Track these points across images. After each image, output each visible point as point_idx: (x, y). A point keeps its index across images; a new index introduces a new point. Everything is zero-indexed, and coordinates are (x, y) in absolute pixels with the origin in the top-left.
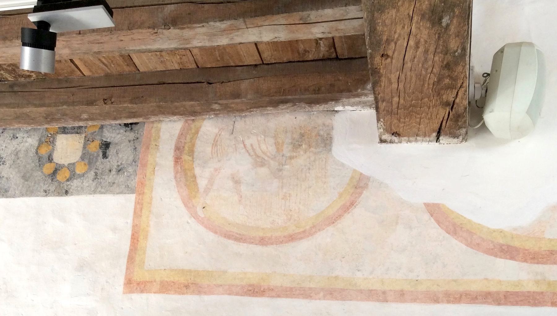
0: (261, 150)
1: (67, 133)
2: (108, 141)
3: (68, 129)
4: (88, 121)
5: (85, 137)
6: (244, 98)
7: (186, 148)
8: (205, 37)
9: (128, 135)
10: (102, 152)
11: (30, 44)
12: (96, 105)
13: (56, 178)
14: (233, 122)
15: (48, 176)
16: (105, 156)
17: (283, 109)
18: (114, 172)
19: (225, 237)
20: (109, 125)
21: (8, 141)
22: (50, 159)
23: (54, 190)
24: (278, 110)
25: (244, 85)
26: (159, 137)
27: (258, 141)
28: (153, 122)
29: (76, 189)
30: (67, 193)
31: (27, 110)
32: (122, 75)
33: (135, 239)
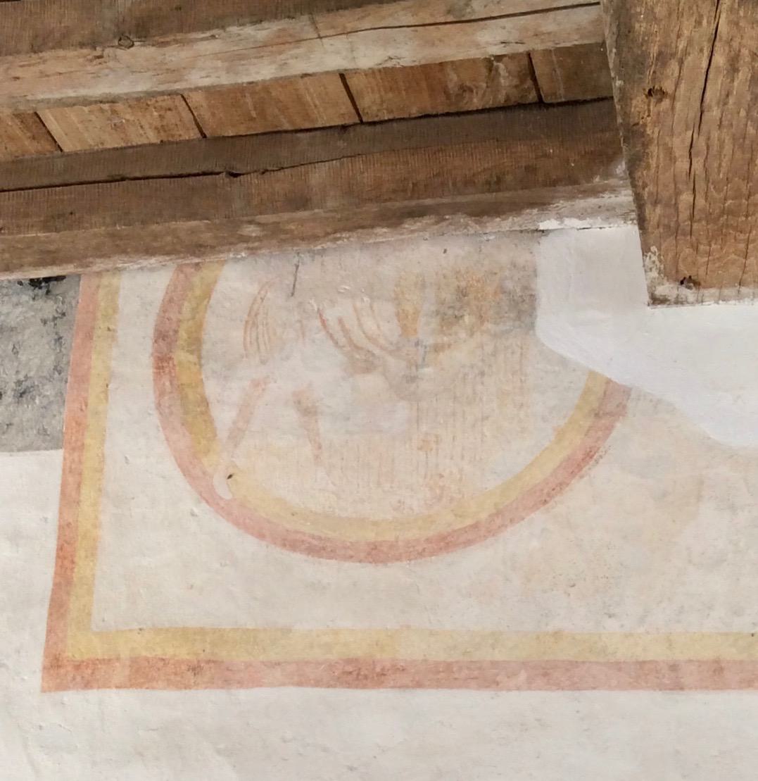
0: (364, 333)
6: (319, 208)
7: (183, 334)
8: (219, 64)
9: (39, 308)
14: (295, 268)
17: (413, 232)
19: (284, 545)
24: (402, 234)
25: (318, 176)
26: (115, 310)
28: (99, 274)
33: (65, 558)
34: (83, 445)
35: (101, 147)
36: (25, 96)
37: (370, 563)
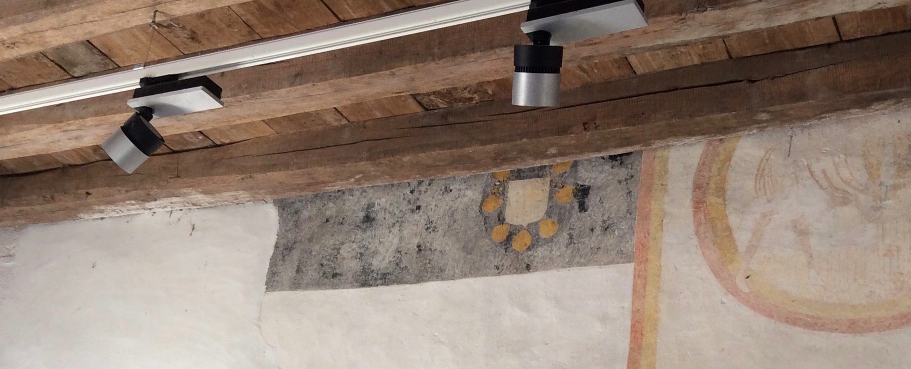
0: (841, 178)
1: (523, 178)
2: (585, 185)
3: (524, 172)
4: (556, 157)
5: (551, 181)
6: (812, 100)
7: (713, 186)
8: (761, 16)
9: (616, 173)
10: (578, 202)
11: (528, 68)
12: (571, 133)
13: (512, 246)
14: (790, 138)
15: (500, 245)
16: (583, 208)
17: (877, 110)
18: (598, 231)
19: (787, 322)
20: (587, 160)
21: (439, 196)
22: (501, 220)
23: (510, 265)
24: (869, 112)
25: (812, 78)
26: (666, 172)
27: (835, 164)
28: (655, 150)
29: (542, 260)
30: (528, 268)
31: (469, 150)
32: (609, 82)
33: (637, 332)
34: (647, 259)
35: (661, 69)
36: (630, 46)
37: (851, 333)
